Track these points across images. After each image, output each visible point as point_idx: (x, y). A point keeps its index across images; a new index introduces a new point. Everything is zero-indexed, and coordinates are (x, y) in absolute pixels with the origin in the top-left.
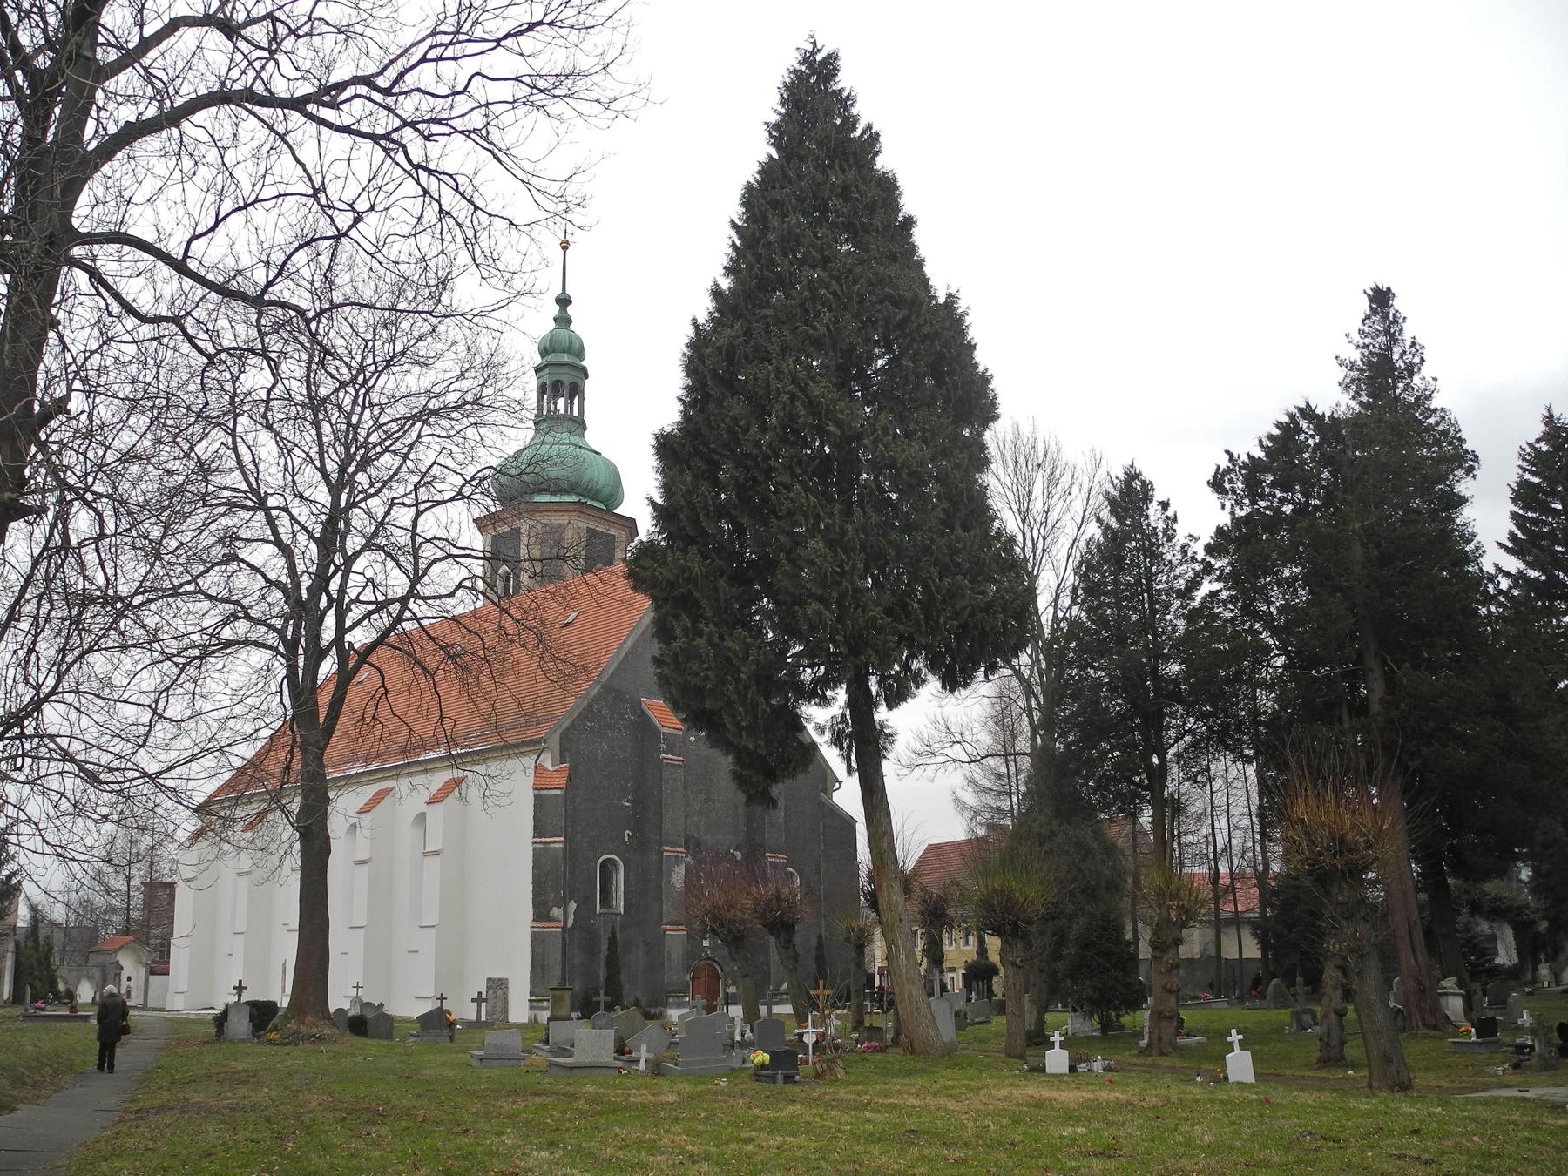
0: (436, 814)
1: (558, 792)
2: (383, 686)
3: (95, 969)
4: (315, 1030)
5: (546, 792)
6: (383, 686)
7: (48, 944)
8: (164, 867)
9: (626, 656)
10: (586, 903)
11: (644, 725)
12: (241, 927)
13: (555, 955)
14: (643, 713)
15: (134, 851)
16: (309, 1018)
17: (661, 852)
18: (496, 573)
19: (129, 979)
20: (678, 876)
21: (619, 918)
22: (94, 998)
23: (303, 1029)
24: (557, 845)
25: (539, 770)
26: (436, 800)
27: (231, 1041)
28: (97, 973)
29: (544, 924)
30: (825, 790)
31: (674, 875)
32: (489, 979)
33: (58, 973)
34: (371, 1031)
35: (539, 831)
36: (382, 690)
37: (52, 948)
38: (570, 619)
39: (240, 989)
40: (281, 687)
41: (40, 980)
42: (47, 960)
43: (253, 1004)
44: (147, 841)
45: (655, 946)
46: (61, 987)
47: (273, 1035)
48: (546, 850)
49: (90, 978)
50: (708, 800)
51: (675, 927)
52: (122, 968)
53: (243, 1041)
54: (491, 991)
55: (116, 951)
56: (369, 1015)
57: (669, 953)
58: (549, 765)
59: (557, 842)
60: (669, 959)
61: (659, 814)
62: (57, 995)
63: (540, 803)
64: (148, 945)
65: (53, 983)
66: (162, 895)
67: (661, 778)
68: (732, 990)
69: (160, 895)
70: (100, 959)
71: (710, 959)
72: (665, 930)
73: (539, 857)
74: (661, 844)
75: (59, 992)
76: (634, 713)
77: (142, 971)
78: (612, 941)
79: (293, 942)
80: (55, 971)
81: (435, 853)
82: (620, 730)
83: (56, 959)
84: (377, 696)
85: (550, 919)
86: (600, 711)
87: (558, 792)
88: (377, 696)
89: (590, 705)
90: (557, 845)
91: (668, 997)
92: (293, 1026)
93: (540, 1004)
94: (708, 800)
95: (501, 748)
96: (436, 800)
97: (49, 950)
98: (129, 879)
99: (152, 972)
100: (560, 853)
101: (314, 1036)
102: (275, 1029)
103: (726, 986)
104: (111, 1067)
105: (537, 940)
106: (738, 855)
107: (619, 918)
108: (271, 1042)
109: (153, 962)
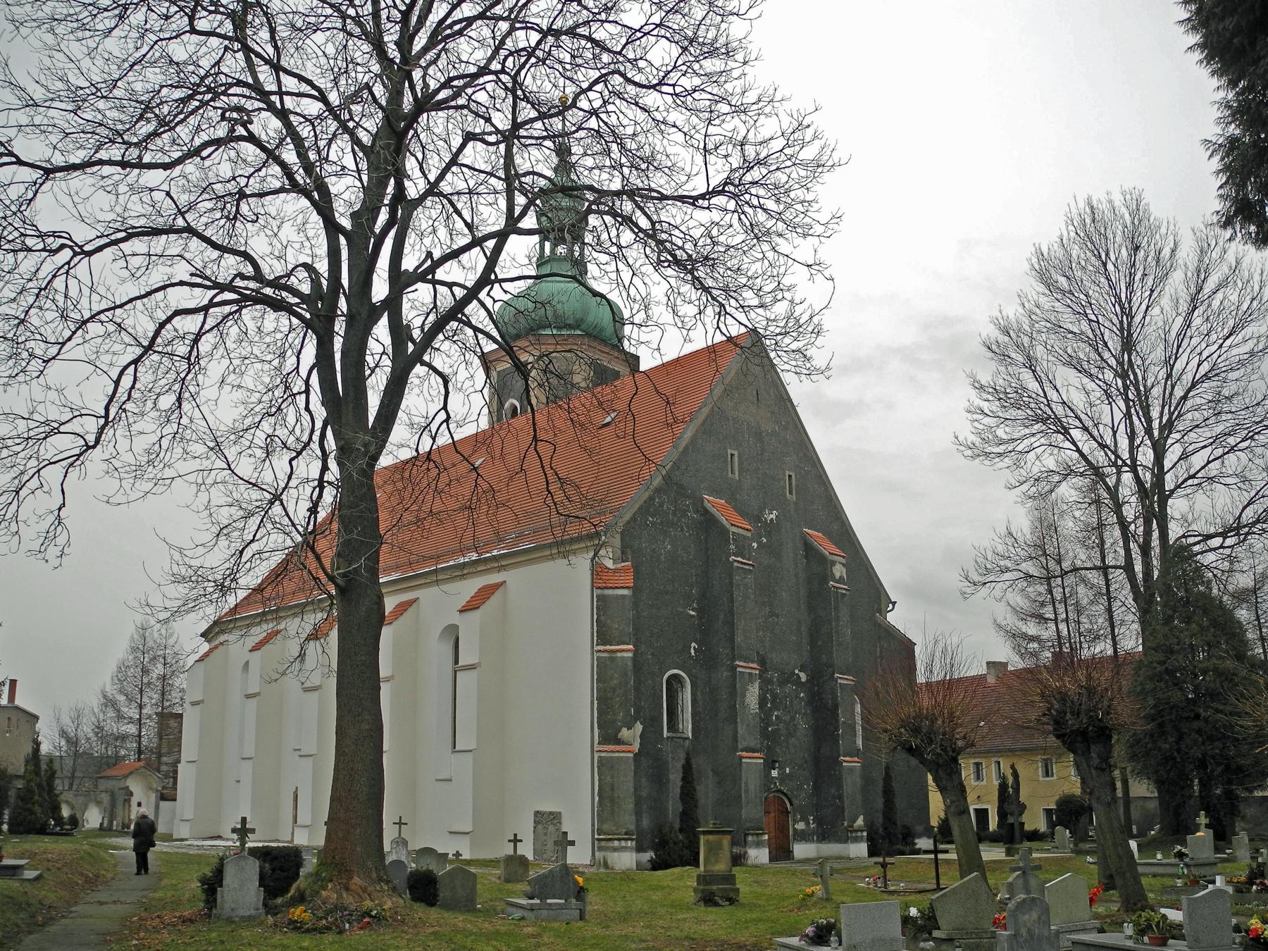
0: (470, 627)
1: (625, 592)
2: (445, 408)
3: (103, 795)
4: (368, 903)
5: (610, 592)
6: (445, 408)
7: (51, 768)
8: (175, 696)
9: (687, 447)
10: (652, 725)
11: (708, 522)
12: (249, 751)
13: (626, 783)
14: (706, 511)
15: (145, 680)
16: (357, 881)
17: (734, 668)
18: (503, 406)
19: (139, 804)
20: (752, 695)
21: (687, 743)
22: (102, 824)
23: (348, 899)
24: (625, 655)
25: (597, 571)
26: (471, 607)
27: (230, 921)
28: (105, 798)
29: (612, 747)
30: (880, 611)
31: (748, 695)
32: (537, 813)
33: (63, 797)
34: (443, 894)
35: (603, 635)
36: (442, 415)
37: (54, 772)
38: (608, 419)
39: (243, 831)
40: (307, 382)
41: (41, 806)
42: (51, 788)
43: (264, 854)
44: (158, 670)
45: (729, 776)
46: (66, 812)
47: (298, 912)
48: (612, 659)
49: (99, 803)
50: (772, 614)
51: (750, 754)
52: (131, 794)
53: (249, 920)
54: (540, 827)
55: (126, 777)
56: (441, 871)
57: (746, 784)
58: (609, 564)
59: (626, 651)
60: (747, 791)
61: (731, 625)
62: (59, 821)
63: (603, 606)
64: (159, 771)
65: (56, 808)
66: (173, 723)
67: (731, 583)
68: (801, 826)
69: (169, 722)
70: (110, 784)
71: (780, 791)
72: (741, 758)
73: (603, 670)
74: (734, 659)
75: (62, 818)
76: (697, 511)
77: (153, 796)
78: (687, 769)
79: (386, 746)
80: (57, 796)
81: (472, 667)
82: (682, 530)
83: (59, 785)
84: (434, 427)
85: (619, 742)
86: (661, 505)
87: (625, 592)
88: (434, 427)
89: (651, 498)
90: (625, 655)
91: (746, 835)
92: (330, 894)
93: (610, 844)
94: (772, 614)
95: (550, 546)
96: (471, 607)
97: (52, 775)
98: (141, 707)
99: (163, 798)
100: (630, 664)
101: (367, 913)
102: (301, 899)
103: (795, 822)
104: (146, 870)
105: (605, 767)
106: (803, 677)
107: (687, 743)
108: (296, 926)
109: (164, 788)
